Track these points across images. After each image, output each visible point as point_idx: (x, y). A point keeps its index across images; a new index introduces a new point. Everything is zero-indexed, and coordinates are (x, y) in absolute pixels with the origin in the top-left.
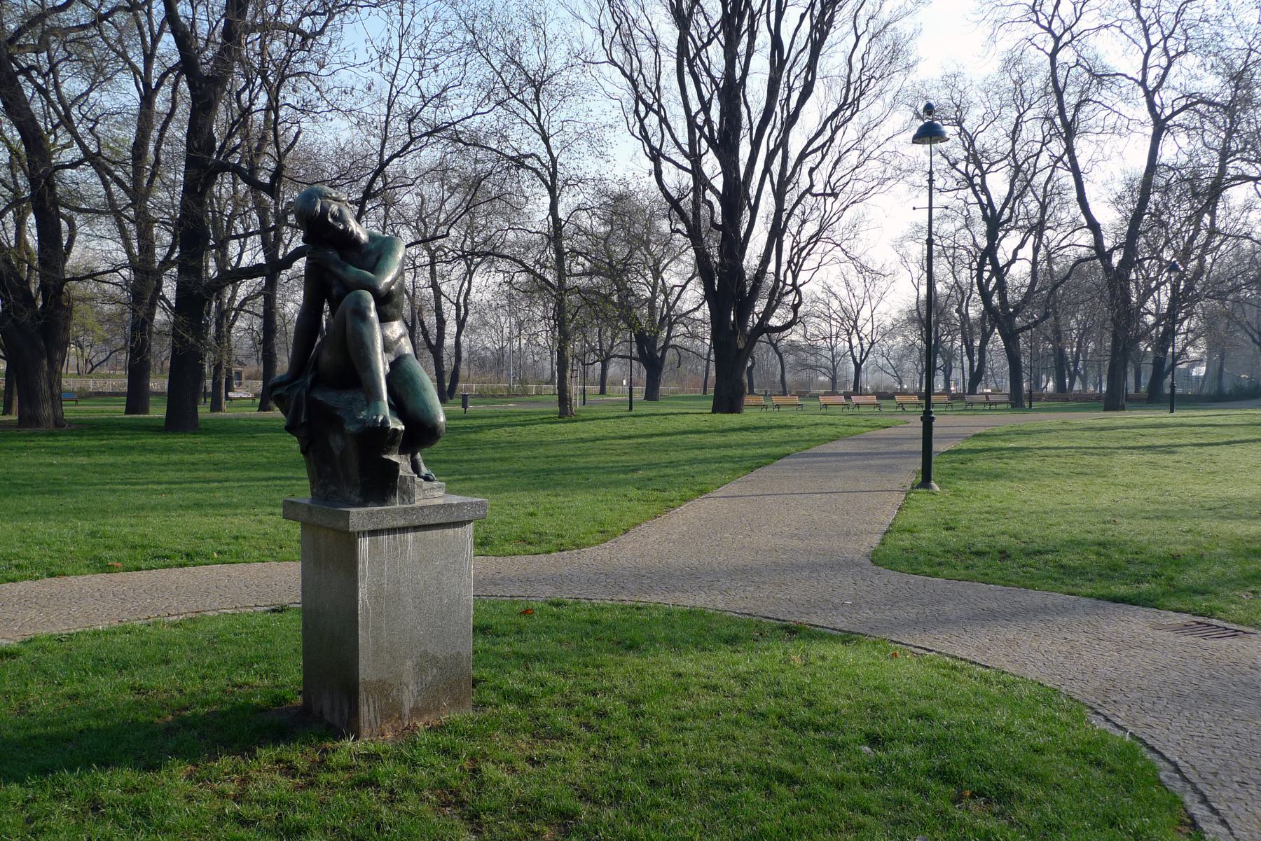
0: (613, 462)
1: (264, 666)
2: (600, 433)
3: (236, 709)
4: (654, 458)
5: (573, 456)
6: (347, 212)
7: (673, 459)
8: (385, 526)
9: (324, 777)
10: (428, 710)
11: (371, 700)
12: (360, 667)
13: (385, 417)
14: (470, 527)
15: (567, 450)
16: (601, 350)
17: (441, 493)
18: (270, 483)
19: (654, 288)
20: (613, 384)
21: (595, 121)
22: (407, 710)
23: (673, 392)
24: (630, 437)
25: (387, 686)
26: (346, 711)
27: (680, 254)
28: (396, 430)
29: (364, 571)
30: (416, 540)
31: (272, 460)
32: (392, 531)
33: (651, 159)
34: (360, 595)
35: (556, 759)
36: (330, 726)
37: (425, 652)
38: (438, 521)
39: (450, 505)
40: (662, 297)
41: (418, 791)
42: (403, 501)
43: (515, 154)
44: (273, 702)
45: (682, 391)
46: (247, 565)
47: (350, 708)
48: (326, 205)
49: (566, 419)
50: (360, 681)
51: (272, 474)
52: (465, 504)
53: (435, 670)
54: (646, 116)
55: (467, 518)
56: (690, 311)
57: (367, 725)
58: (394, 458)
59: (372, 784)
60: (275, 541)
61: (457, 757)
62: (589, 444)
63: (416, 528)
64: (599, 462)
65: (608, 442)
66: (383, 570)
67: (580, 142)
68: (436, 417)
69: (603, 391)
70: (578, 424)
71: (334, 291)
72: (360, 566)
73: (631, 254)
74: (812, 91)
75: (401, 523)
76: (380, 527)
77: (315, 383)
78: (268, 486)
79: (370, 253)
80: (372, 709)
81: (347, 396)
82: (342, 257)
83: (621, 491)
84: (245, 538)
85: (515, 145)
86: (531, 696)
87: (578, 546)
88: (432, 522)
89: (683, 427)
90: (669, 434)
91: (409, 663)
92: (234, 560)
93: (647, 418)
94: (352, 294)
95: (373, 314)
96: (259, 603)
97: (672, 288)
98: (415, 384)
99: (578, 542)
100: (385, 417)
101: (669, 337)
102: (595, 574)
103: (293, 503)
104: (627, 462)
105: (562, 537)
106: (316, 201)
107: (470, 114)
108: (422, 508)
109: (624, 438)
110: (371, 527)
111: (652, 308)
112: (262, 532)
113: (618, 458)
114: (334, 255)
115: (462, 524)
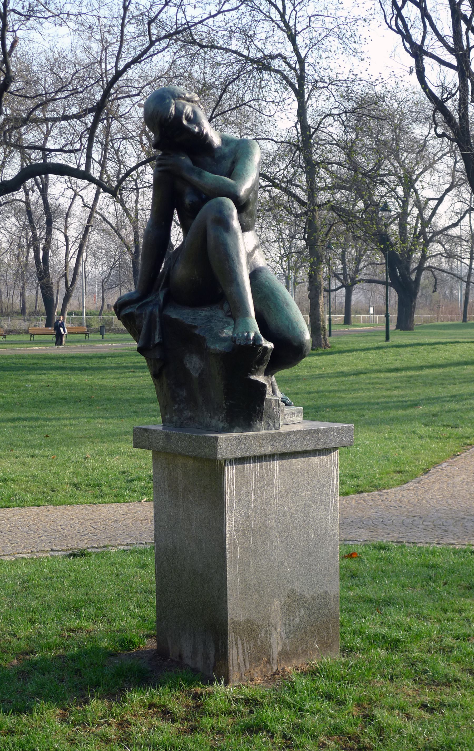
0: (385, 397)
1: (92, 610)
2: (361, 366)
3: (84, 653)
4: (431, 392)
5: (338, 391)
6: (201, 113)
7: (454, 392)
8: (253, 453)
9: (207, 722)
10: (296, 655)
11: (239, 642)
12: (229, 606)
13: (256, 334)
14: (335, 454)
15: (331, 385)
16: (344, 274)
17: (300, 419)
18: (17, 424)
19: (405, 203)
20: (357, 312)
21: (346, 14)
22: (275, 655)
23: (426, 321)
24: (397, 370)
25: (255, 627)
26: (212, 654)
27: (435, 162)
28: (266, 348)
29: (231, 502)
30: (282, 469)
31: (9, 400)
32: (259, 458)
33: (411, 55)
34: (228, 528)
35: (450, 707)
36: (195, 671)
37: (293, 591)
38: (305, 448)
39: (317, 431)
40: (416, 211)
41: (314, 737)
42: (268, 427)
43: (260, 55)
44: (121, 645)
45: (438, 319)
46: (23, 509)
47: (217, 651)
48: (180, 106)
49: (320, 351)
50: (229, 621)
51: (14, 415)
52: (332, 430)
53: (302, 611)
54: (403, 6)
55: (333, 445)
56: (449, 227)
57: (236, 669)
58: (261, 379)
59: (261, 729)
60: (46, 484)
61: (341, 703)
62: (351, 378)
63: (283, 456)
64: (370, 398)
65: (373, 375)
66: (250, 501)
67: (331, 39)
68: (301, 334)
69: (347, 321)
70: (336, 357)
71: (188, 201)
72: (227, 497)
73: (378, 165)
75: (268, 450)
76: (248, 454)
77: (169, 299)
78: (16, 427)
79: (223, 157)
80: (240, 651)
81: (203, 313)
82: (194, 163)
83: (408, 427)
84: (13, 480)
85: (260, 45)
86: (399, 641)
87: (377, 487)
88: (299, 449)
89: (456, 358)
90: (441, 366)
91: (277, 603)
92: (8, 504)
93: (413, 349)
94: (213, 201)
95: (236, 224)
96: (54, 548)
97: (426, 203)
98: (276, 298)
99: (376, 482)
100: (256, 334)
101: (424, 258)
102: (408, 517)
103: (146, 430)
104: (402, 396)
105: (357, 477)
106: (170, 102)
107: (213, 13)
108: (288, 434)
109: (390, 371)
110: (239, 454)
111: (402, 226)
112: (29, 474)
113: (388, 393)
114: (185, 160)
115: (327, 451)
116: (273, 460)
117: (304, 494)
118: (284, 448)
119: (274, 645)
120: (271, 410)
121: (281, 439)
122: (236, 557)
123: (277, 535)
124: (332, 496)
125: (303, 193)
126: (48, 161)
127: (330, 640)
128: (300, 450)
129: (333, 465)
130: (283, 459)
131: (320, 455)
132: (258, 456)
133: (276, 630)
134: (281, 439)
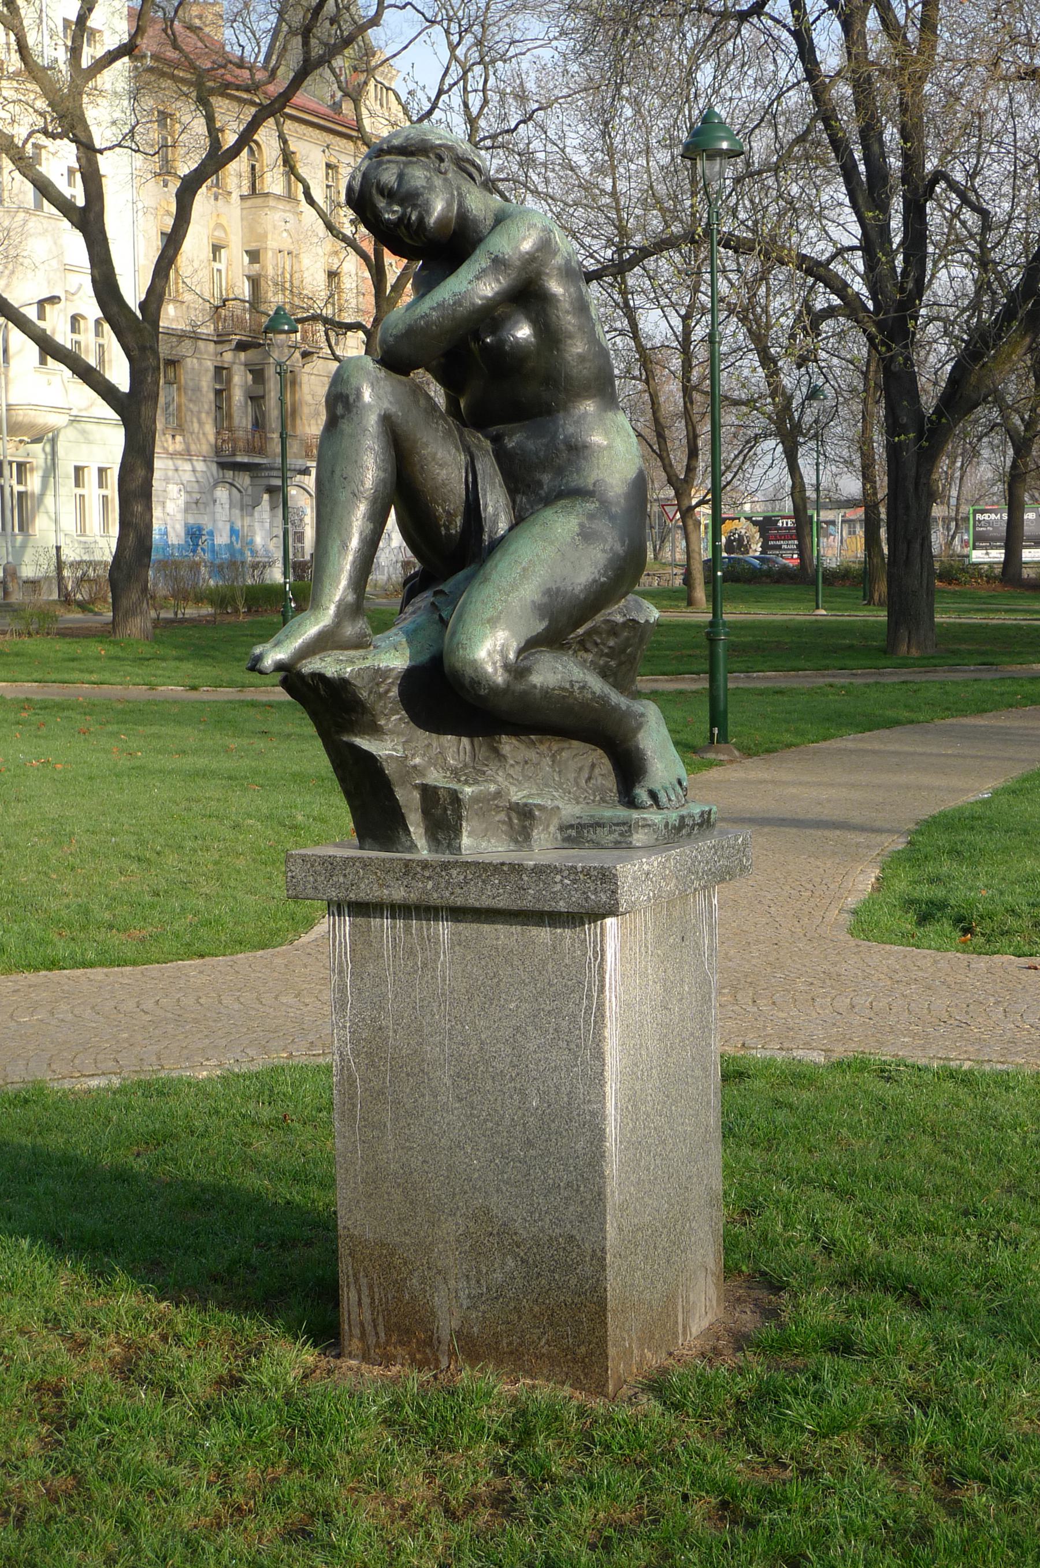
30: (457, 941)
38: (486, 902)
50: (341, 1232)
53: (510, 1262)
57: (357, 1331)
63: (458, 913)
66: (383, 996)
74: (177, 195)
80: (366, 1301)
88: (472, 902)
116: (436, 919)
117: (512, 1006)
118: (435, 895)
119: (442, 1314)
120: (439, 811)
121: (427, 874)
122: (354, 1106)
123: (446, 1080)
124: (586, 1022)
125: (858, 279)
126: (247, 299)
127: (583, 1349)
128: (477, 905)
129: (590, 953)
130: (459, 921)
131: (479, 921)
132: (400, 906)
133: (446, 1283)
134: (427, 874)
